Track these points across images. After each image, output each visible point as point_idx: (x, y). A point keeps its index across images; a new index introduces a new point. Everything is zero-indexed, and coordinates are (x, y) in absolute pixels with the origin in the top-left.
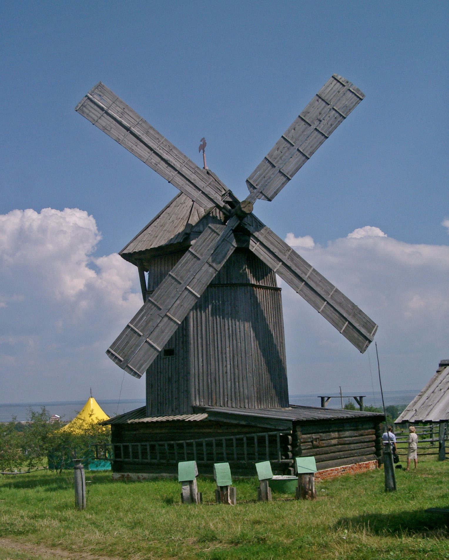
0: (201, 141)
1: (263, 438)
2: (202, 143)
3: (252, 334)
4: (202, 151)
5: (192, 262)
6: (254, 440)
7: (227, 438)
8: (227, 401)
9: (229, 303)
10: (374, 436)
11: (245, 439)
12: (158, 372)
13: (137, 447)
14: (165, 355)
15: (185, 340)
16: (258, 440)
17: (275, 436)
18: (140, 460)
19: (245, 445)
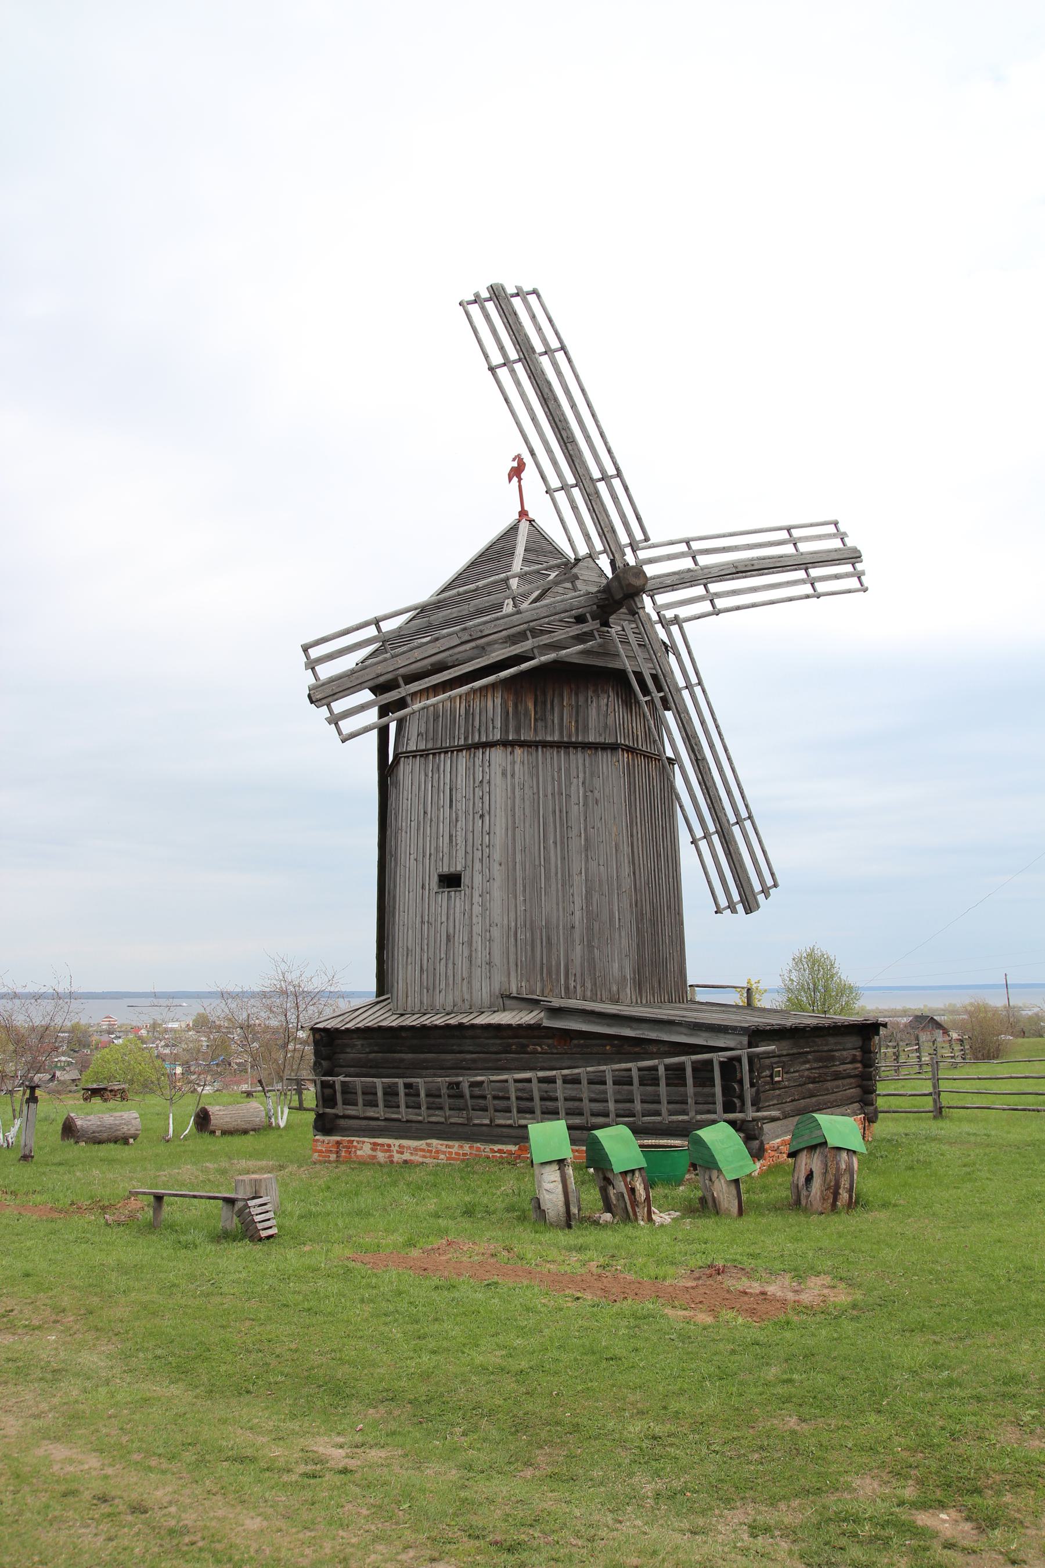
0: (514, 460)
1: (681, 1068)
2: (515, 464)
3: (452, 1022)
4: (515, 479)
5: (478, 762)
6: (684, 1069)
7: (541, 1074)
8: (575, 987)
9: (581, 780)
10: (859, 1065)
11: (661, 1070)
12: (422, 922)
13: (374, 1073)
14: (440, 887)
15: (486, 855)
16: (694, 1070)
17: (710, 1062)
18: (380, 1112)
19: (663, 1082)
